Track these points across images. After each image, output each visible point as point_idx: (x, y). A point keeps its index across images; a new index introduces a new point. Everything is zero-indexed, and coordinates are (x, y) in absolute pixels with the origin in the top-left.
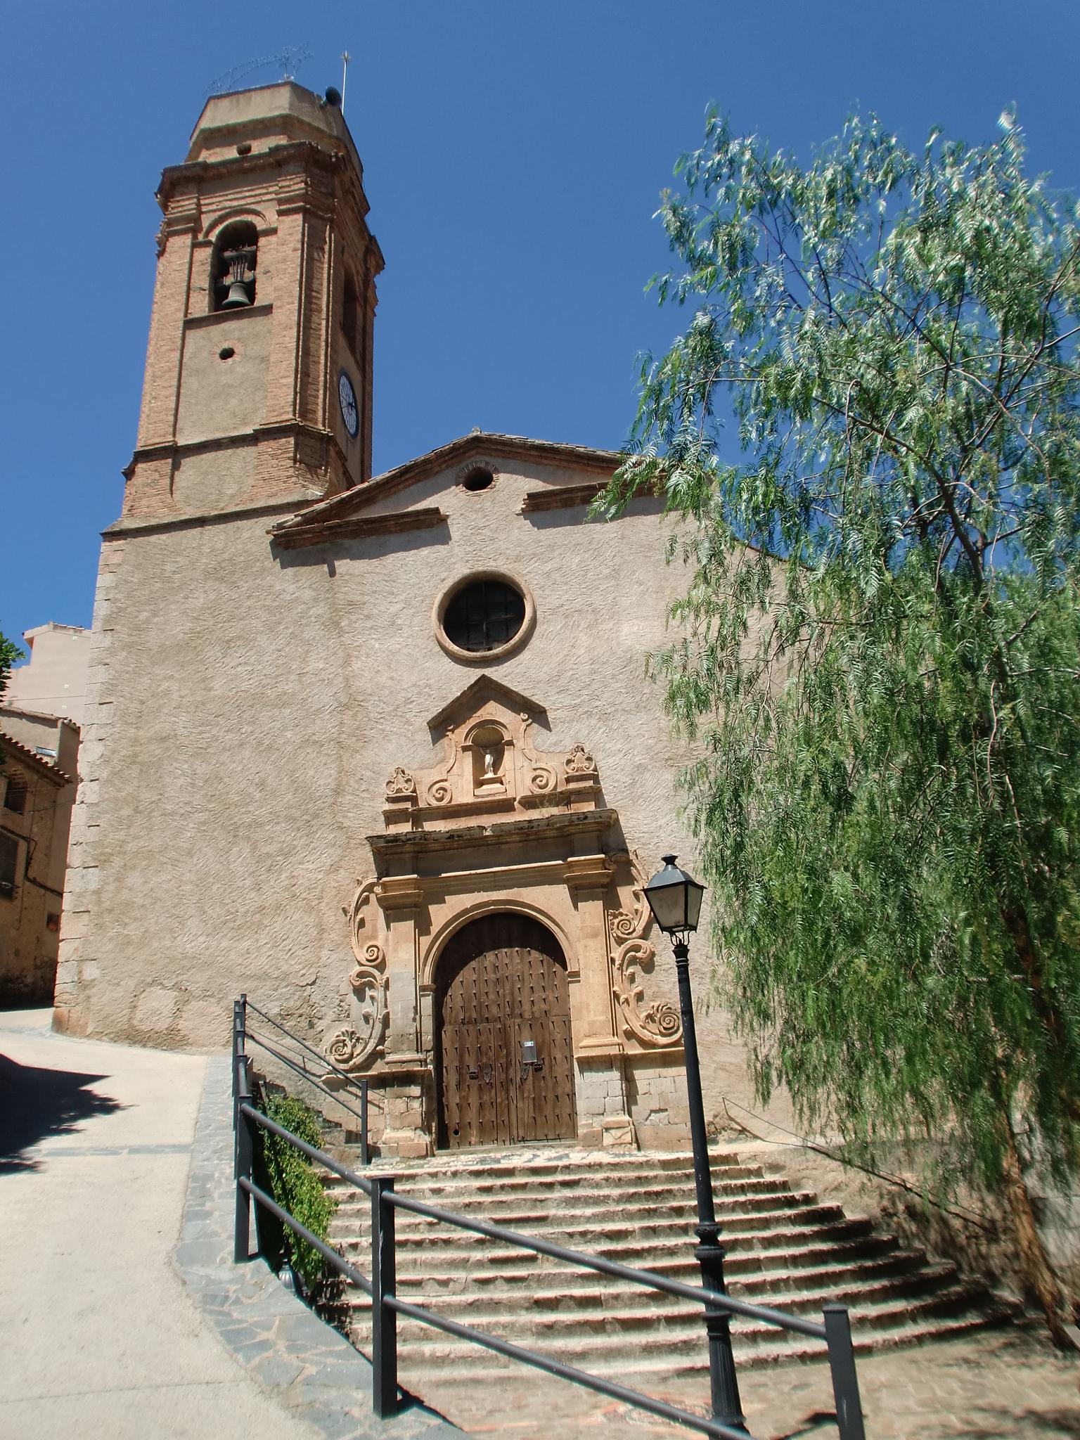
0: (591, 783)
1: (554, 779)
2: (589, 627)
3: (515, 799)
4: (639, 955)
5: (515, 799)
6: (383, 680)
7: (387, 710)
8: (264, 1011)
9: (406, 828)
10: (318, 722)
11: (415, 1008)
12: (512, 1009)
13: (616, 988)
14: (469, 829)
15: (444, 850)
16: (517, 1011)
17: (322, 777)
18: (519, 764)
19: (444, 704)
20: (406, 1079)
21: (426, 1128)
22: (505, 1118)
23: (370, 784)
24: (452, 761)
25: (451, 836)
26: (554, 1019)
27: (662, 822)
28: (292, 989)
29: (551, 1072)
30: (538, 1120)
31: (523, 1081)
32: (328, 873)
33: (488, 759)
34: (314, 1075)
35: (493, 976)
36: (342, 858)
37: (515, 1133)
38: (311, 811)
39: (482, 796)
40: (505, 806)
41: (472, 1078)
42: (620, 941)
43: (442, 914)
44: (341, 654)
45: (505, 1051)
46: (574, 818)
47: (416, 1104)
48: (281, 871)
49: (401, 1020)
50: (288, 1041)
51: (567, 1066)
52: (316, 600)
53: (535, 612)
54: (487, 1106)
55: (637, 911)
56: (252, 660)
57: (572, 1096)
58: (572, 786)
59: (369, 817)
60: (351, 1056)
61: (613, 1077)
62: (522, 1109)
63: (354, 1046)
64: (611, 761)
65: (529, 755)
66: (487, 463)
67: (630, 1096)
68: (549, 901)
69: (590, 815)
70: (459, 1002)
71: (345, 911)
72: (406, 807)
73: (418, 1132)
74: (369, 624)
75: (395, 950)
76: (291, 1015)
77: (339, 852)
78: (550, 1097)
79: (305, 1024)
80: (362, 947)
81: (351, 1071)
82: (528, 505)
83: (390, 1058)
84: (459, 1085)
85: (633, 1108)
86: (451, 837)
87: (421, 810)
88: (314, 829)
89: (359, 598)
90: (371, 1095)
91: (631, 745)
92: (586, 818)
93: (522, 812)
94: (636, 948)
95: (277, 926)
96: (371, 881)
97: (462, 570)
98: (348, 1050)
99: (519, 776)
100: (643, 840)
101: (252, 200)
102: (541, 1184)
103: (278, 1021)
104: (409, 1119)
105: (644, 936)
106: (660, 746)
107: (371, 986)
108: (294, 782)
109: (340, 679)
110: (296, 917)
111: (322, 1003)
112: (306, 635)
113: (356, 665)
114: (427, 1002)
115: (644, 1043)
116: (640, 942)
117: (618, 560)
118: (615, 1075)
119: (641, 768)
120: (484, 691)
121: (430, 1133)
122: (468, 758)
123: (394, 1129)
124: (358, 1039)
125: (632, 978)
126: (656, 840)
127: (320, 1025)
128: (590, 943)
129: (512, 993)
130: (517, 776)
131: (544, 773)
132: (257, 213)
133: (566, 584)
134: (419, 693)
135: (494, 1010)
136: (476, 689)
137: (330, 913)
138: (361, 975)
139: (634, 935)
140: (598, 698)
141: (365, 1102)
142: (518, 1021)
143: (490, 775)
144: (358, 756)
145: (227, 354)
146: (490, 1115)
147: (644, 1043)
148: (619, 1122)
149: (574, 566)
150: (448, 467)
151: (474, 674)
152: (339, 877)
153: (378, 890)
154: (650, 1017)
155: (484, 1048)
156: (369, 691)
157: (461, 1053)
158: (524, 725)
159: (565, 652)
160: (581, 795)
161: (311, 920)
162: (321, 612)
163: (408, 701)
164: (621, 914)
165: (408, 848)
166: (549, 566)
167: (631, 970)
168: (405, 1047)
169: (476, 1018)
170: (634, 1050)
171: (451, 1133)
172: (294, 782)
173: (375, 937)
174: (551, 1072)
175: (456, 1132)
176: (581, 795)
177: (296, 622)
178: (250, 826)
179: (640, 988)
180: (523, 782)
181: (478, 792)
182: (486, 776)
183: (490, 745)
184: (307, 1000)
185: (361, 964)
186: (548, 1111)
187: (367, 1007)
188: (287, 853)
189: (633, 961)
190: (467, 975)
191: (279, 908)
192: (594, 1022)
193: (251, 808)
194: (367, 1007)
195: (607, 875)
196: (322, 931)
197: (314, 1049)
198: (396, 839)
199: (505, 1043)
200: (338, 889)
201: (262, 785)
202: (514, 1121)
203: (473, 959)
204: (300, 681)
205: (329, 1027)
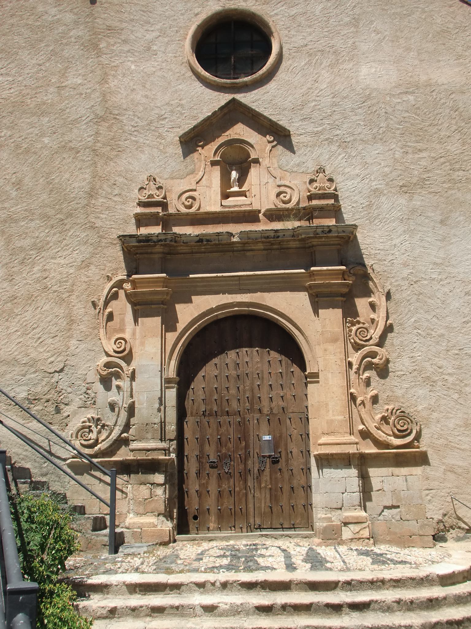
0: (332, 201)
1: (297, 196)
2: (331, 66)
3: (259, 211)
4: (375, 361)
5: (259, 211)
6: (138, 97)
7: (141, 124)
8: (12, 395)
9: (156, 230)
10: (75, 131)
11: (160, 399)
12: (252, 404)
13: (352, 390)
14: (218, 234)
15: (192, 253)
16: (257, 407)
17: (78, 181)
19: (194, 123)
20: (148, 467)
21: (168, 515)
22: (243, 506)
23: (122, 189)
24: (201, 174)
25: (200, 240)
26: (291, 415)
27: (397, 241)
28: (40, 375)
29: (287, 464)
30: (274, 509)
31: (261, 472)
32: (79, 268)
33: (234, 175)
34: (59, 458)
35: (233, 373)
36: (93, 255)
37: (252, 521)
38: (65, 211)
39: (229, 207)
40: (251, 216)
41: (212, 467)
42: (357, 347)
43: (187, 313)
44: (99, 72)
45: (244, 444)
46: (319, 231)
47: (159, 491)
48: (33, 264)
49: (147, 409)
50: (34, 425)
51: (302, 460)
52: (76, 23)
53: (281, 48)
54: (226, 494)
55: (373, 321)
56: (13, 72)
57: (307, 488)
58: (315, 202)
59: (122, 216)
60: (96, 442)
61: (351, 474)
62: (260, 499)
63: (99, 432)
64: (349, 183)
65: (273, 172)
67: (366, 492)
68: (291, 306)
69: (334, 229)
70: (201, 395)
71: (94, 304)
72: (154, 210)
73: (162, 518)
74: (126, 48)
75: (142, 344)
76: (39, 400)
77: (91, 249)
78: (286, 488)
79: (52, 409)
80: (109, 339)
81: (95, 456)
83: (134, 445)
84: (198, 474)
85: (368, 504)
86: (201, 241)
87: (171, 215)
88: (67, 227)
89: (117, 24)
90: (121, 480)
91: (368, 171)
92: (330, 231)
93: (266, 224)
94: (373, 355)
95: (28, 315)
96: (120, 277)
98: (93, 436)
99: (264, 191)
100: (379, 257)
102: (329, 606)
103: (26, 405)
104: (153, 505)
105: (380, 344)
106: (395, 174)
107: (118, 376)
108: (49, 183)
109: (97, 94)
110: (46, 307)
111: (69, 390)
112: (66, 53)
113: (113, 83)
114: (172, 394)
115: (377, 443)
116: (376, 349)
117: (357, 11)
118: (353, 472)
119: (377, 192)
120: (233, 113)
121: (172, 519)
122: (216, 173)
123: (138, 514)
124: (103, 426)
125: (368, 383)
126: (390, 257)
127: (67, 411)
128: (331, 347)
129: (252, 390)
130: (261, 190)
131: (288, 190)
133: (310, 27)
134: (172, 111)
135: (234, 405)
136: (226, 111)
137: (79, 305)
138: (108, 365)
139: (371, 342)
140: (338, 127)
141: (114, 488)
142: (257, 416)
143: (235, 189)
144: (112, 164)
146: (228, 503)
147: (377, 443)
148: (357, 518)
151: (224, 98)
152: (90, 273)
153: (127, 286)
154: (385, 419)
155: (223, 439)
156: (125, 107)
157: (201, 442)
158: (269, 146)
159: (309, 85)
160: (323, 212)
161: (61, 311)
162: (80, 33)
163: (161, 118)
164: (359, 322)
165: (158, 249)
166: (293, 11)
167: (367, 374)
168: (149, 436)
169: (215, 412)
170: (370, 449)
171: (190, 517)
172: (49, 183)
173: (122, 330)
174: (287, 464)
175: (195, 518)
176: (323, 212)
177: (56, 41)
178: (5, 221)
179: (375, 392)
180: (268, 197)
181: (225, 202)
182: (232, 190)
183: (237, 163)
184: (55, 386)
185: (108, 355)
186: (284, 501)
187: (113, 396)
188: (40, 248)
189: (369, 366)
190: (209, 370)
191: (30, 298)
192: (332, 421)
193: (6, 205)
194: (113, 396)
195: (347, 285)
196: (71, 322)
197: (60, 433)
198: (147, 239)
199: (244, 436)
200: (88, 283)
201: (18, 185)
202: (252, 510)
203: (215, 356)
204: (59, 94)
205: (75, 413)
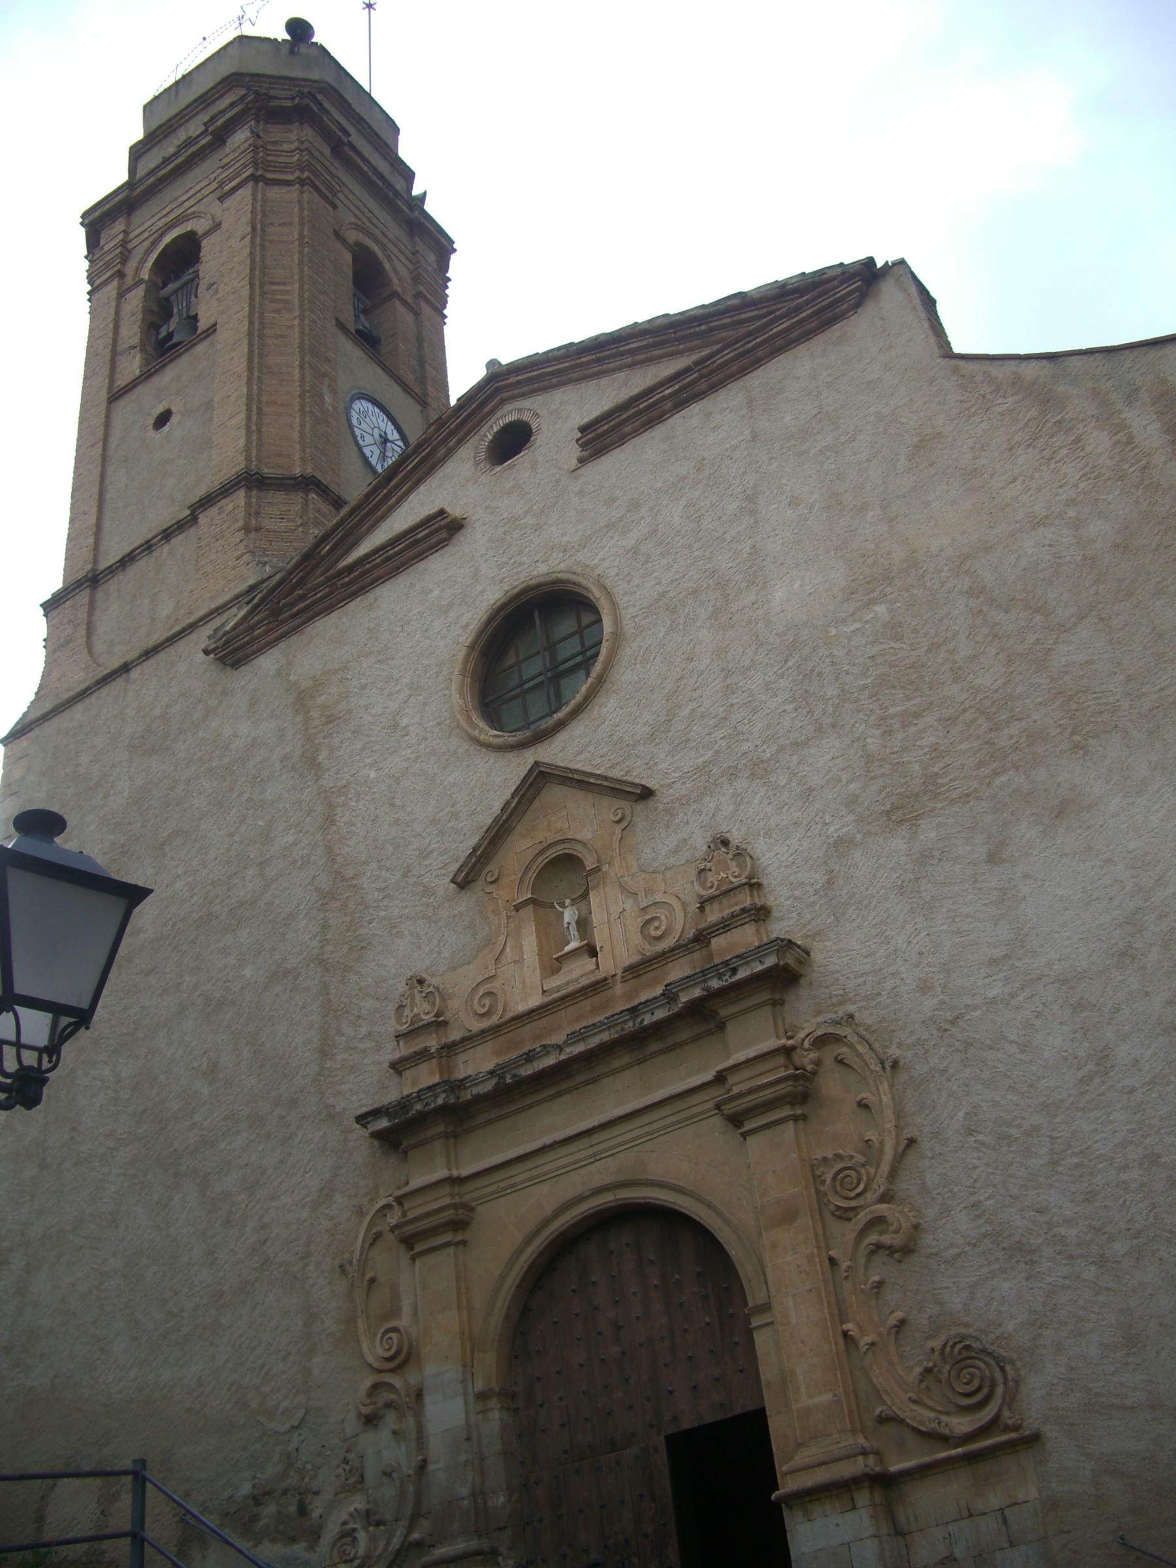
2: (715, 614)
18: (615, 910)
42: (845, 1214)
66: (520, 410)
68: (691, 1164)
82: (584, 446)
94: (878, 1221)
97: (491, 595)
101: (191, 202)
119: (841, 846)
120: (539, 779)
130: (618, 926)
132: (195, 215)
139: (869, 1196)
145: (163, 419)
149: (677, 520)
150: (460, 442)
